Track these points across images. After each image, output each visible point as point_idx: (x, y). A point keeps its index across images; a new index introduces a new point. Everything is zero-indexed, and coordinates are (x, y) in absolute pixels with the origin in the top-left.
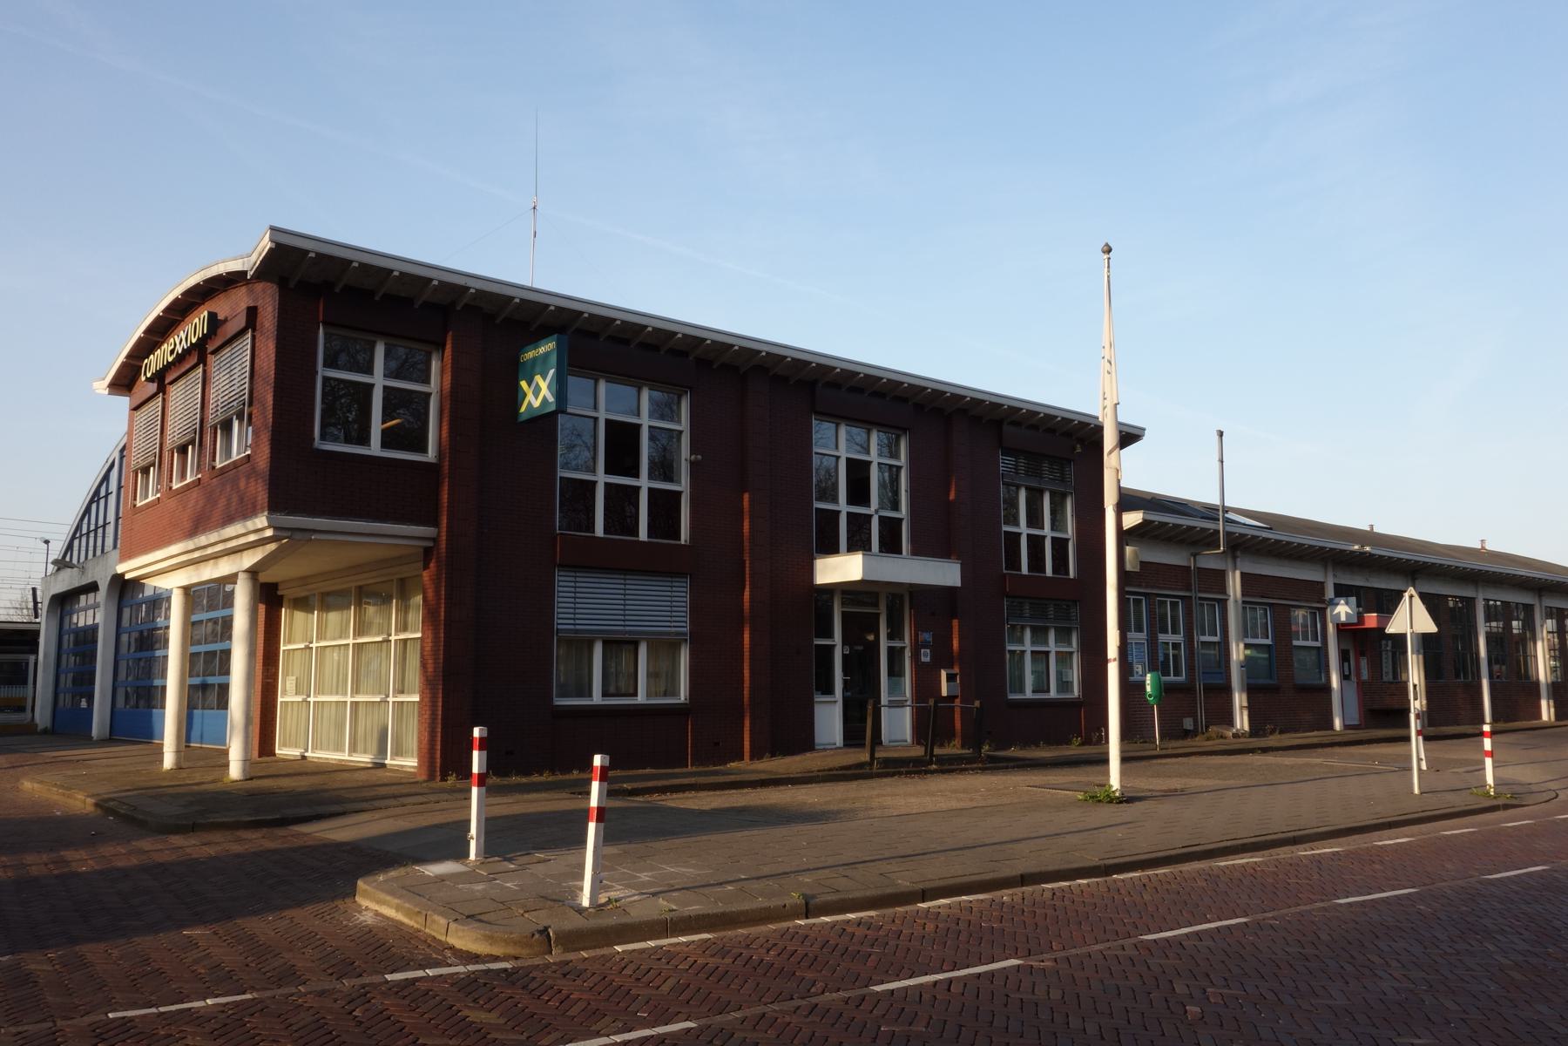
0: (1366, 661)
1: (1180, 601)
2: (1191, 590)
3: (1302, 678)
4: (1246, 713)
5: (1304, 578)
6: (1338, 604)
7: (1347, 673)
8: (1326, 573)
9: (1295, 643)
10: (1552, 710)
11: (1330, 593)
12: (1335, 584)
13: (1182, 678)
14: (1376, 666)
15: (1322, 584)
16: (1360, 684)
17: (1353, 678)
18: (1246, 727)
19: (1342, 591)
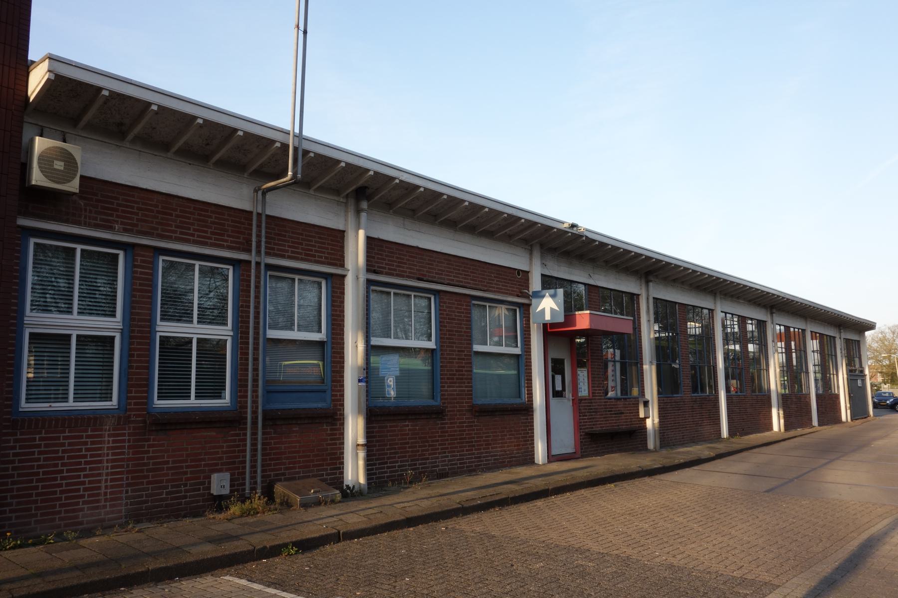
0: (585, 373)
1: (231, 268)
2: (249, 251)
3: (485, 395)
4: (362, 454)
5: (438, 250)
6: (543, 297)
7: (559, 388)
8: (531, 259)
9: (477, 348)
10: (782, 421)
11: (535, 284)
12: (542, 275)
13: (226, 400)
14: (598, 380)
15: (526, 273)
16: (578, 402)
17: (568, 394)
18: (362, 480)
19: (549, 282)
